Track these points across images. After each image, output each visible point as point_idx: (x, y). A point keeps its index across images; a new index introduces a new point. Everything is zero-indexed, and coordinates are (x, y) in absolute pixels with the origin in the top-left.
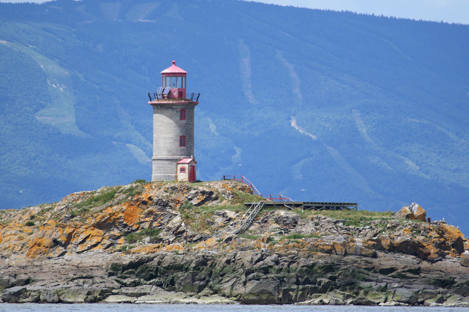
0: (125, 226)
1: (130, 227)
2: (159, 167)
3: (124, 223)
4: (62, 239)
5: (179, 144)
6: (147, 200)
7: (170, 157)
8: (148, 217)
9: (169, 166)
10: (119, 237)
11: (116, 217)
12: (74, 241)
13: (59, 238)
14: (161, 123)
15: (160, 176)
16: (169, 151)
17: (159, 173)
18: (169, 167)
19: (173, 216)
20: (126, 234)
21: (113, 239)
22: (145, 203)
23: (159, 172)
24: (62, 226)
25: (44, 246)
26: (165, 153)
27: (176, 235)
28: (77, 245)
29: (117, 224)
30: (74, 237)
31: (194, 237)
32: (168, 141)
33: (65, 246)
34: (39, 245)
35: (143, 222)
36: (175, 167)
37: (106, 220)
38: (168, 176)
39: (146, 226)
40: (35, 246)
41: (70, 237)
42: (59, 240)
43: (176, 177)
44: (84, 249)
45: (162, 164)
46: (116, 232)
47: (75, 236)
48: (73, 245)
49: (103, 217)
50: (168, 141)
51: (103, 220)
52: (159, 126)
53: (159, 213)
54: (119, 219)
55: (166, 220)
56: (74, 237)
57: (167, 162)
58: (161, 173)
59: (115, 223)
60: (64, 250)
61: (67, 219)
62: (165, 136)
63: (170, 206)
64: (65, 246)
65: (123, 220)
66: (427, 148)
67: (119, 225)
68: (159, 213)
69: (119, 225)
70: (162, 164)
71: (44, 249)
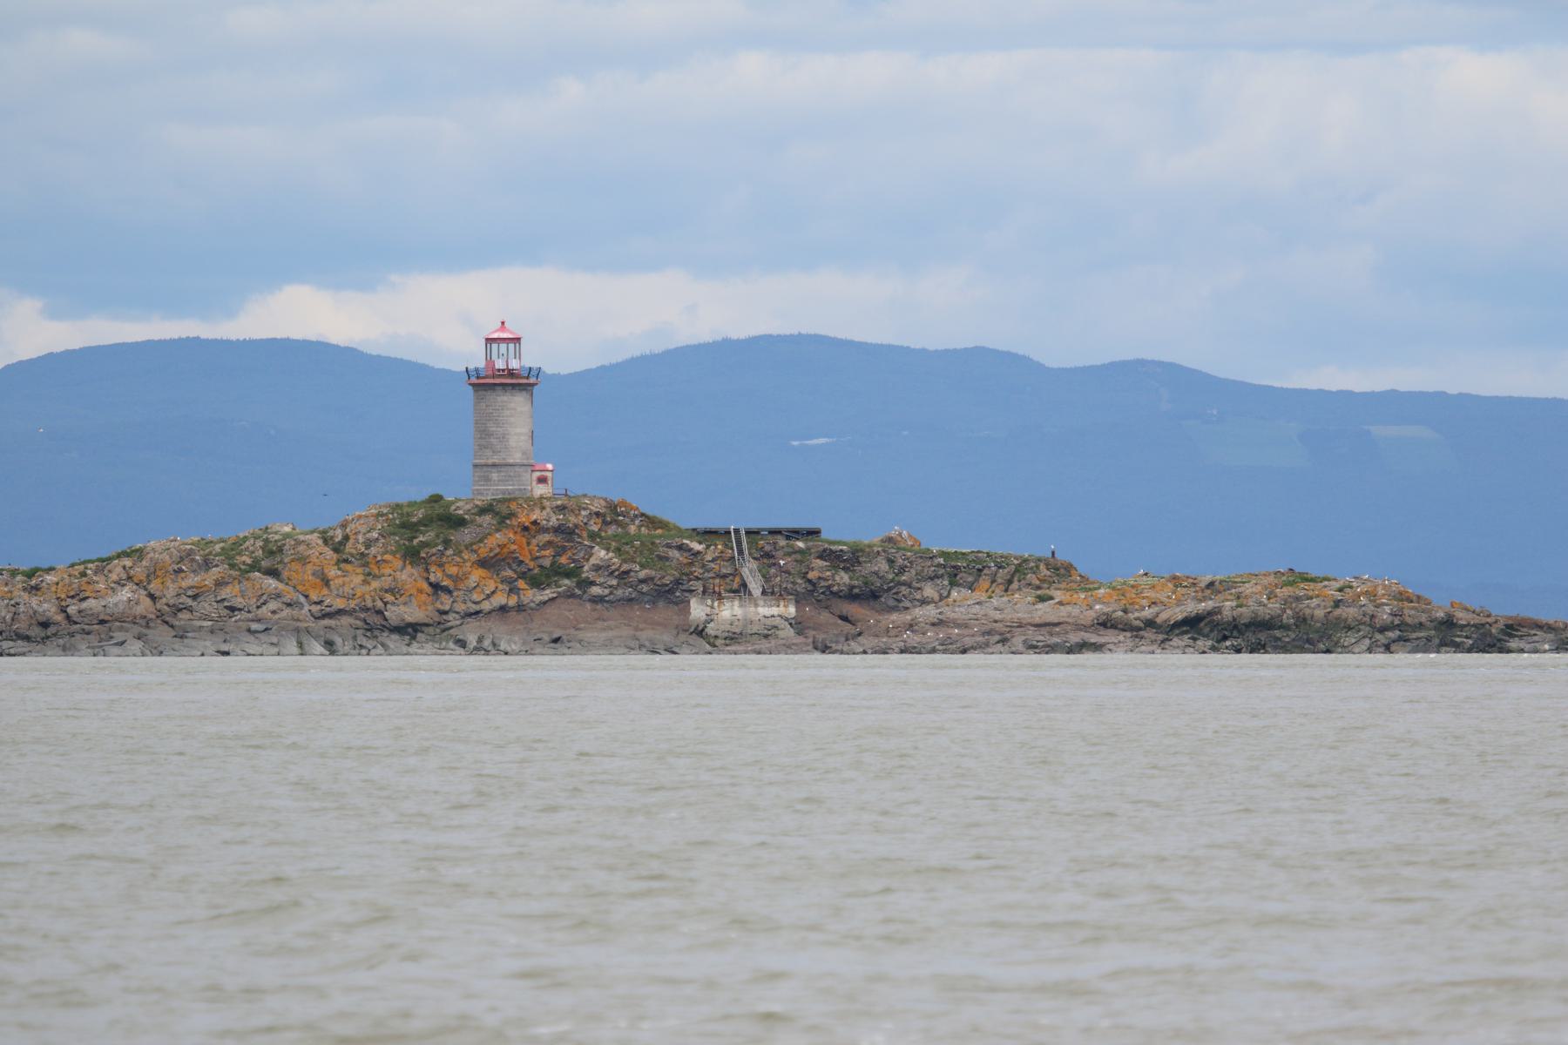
46: (509, 573)
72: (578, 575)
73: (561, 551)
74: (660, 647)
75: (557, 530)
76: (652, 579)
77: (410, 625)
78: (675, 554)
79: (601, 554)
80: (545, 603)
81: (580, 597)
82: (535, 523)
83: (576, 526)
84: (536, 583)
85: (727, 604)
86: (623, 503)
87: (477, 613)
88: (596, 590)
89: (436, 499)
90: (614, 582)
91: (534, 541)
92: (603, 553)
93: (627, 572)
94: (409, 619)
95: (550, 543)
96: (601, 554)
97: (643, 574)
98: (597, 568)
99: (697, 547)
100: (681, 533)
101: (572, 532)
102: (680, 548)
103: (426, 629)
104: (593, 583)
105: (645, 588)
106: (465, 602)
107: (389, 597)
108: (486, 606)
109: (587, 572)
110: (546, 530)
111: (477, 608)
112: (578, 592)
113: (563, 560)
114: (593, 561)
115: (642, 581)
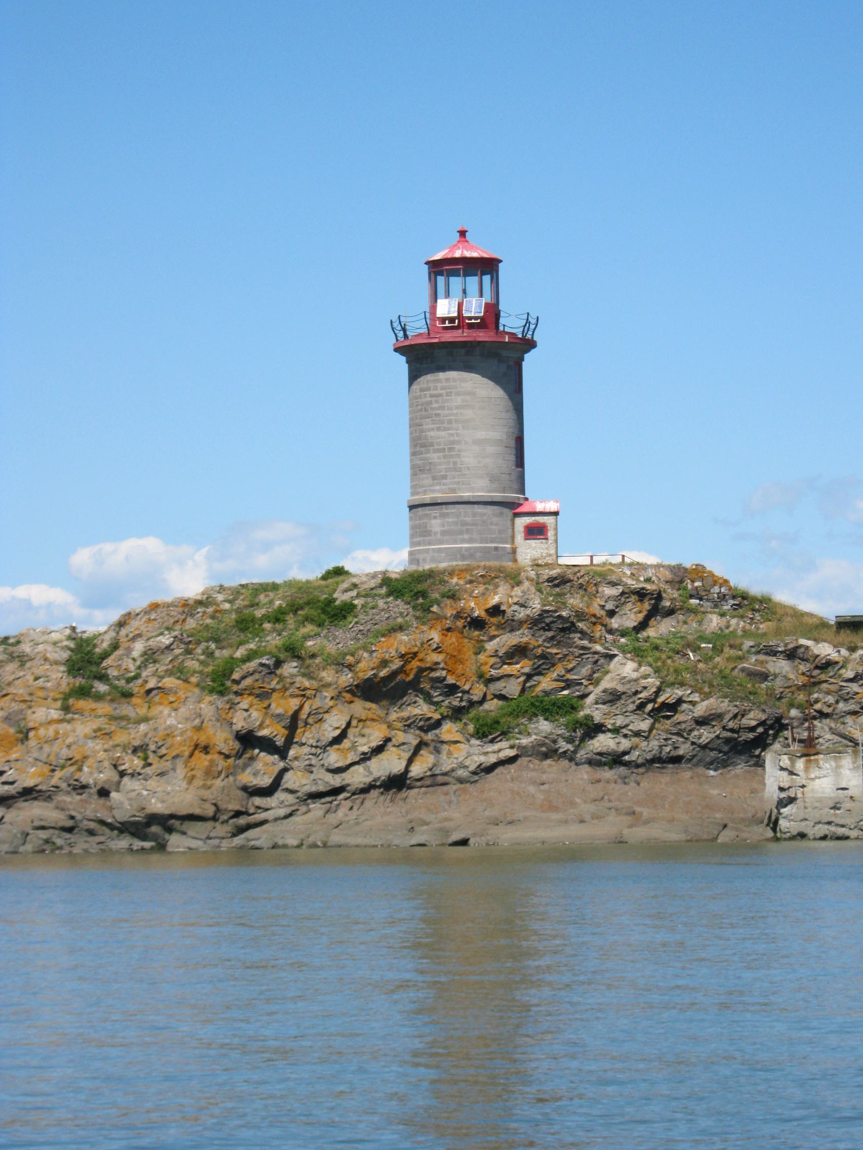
0: (452, 689)
1: (464, 692)
2: (464, 524)
3: (451, 680)
4: (273, 731)
5: (514, 463)
6: (483, 614)
7: (498, 496)
8: (509, 664)
9: (495, 520)
10: (438, 724)
11: (422, 665)
12: (307, 736)
13: (261, 726)
14: (468, 398)
15: (470, 548)
16: (493, 479)
17: (463, 541)
18: (497, 524)
19: (602, 661)
20: (457, 714)
21: (421, 729)
22: (477, 624)
23: (466, 536)
24: (257, 691)
25: (220, 753)
26: (483, 482)
27: (654, 713)
28: (324, 748)
29: (425, 685)
30: (306, 724)
31: (743, 716)
32: (490, 450)
33: (282, 752)
34: (206, 749)
35: (498, 679)
36: (509, 523)
37: (394, 674)
38: (496, 548)
39: (512, 688)
40: (197, 752)
41: (293, 723)
42: (264, 732)
43: (514, 551)
44: (348, 762)
45: (474, 515)
46: (421, 709)
47: (310, 721)
48: (306, 749)
49: (384, 663)
50: (490, 450)
51: (383, 673)
52: (457, 407)
53: (554, 651)
54: (432, 669)
55: (585, 671)
56: (306, 724)
57: (490, 510)
58: (470, 541)
59: (419, 682)
60: (282, 765)
61: (265, 671)
62: (481, 434)
63: (582, 632)
64: (282, 752)
65: (444, 673)
66: (467, 472)
67: (432, 687)
68: (554, 651)
69: (432, 687)
70: (474, 515)
71: (222, 763)
72: (571, 707)
73: (545, 663)
74: (587, 817)
75: (538, 622)
76: (719, 716)
77: (154, 819)
78: (781, 666)
79: (625, 669)
80: (490, 769)
81: (570, 757)
82: (496, 611)
83: (580, 615)
84: (487, 731)
85: (826, 764)
86: (699, 572)
87: (335, 791)
88: (603, 742)
89: (385, 573)
90: (645, 725)
91: (491, 646)
92: (630, 666)
93: (674, 707)
94: (157, 806)
95: (519, 652)
96: (625, 669)
97: (701, 710)
98: (613, 697)
99: (825, 650)
100: (817, 628)
101: (568, 627)
102: (791, 655)
103: (188, 826)
104: (599, 729)
105: (706, 735)
106: (309, 769)
107: (133, 763)
108: (357, 777)
109: (592, 710)
110: (512, 625)
111: (336, 781)
112: (564, 746)
113: (546, 683)
114: (607, 683)
115: (702, 722)
